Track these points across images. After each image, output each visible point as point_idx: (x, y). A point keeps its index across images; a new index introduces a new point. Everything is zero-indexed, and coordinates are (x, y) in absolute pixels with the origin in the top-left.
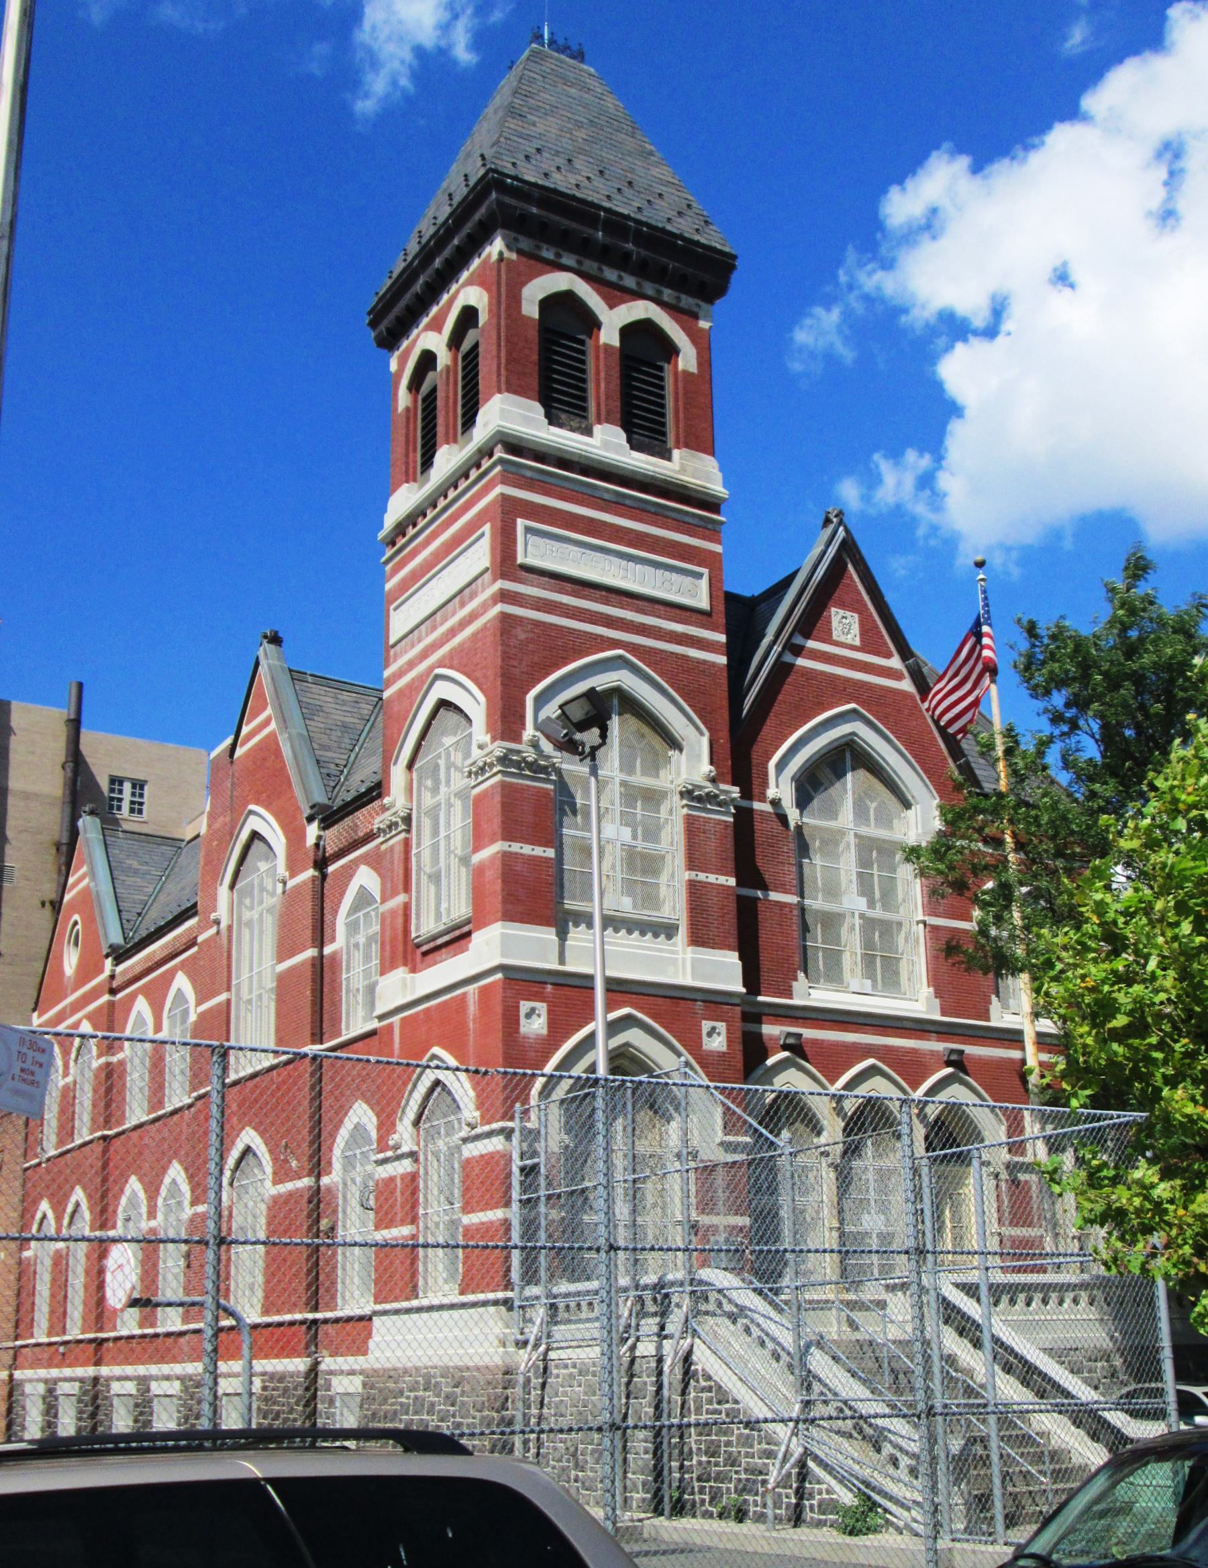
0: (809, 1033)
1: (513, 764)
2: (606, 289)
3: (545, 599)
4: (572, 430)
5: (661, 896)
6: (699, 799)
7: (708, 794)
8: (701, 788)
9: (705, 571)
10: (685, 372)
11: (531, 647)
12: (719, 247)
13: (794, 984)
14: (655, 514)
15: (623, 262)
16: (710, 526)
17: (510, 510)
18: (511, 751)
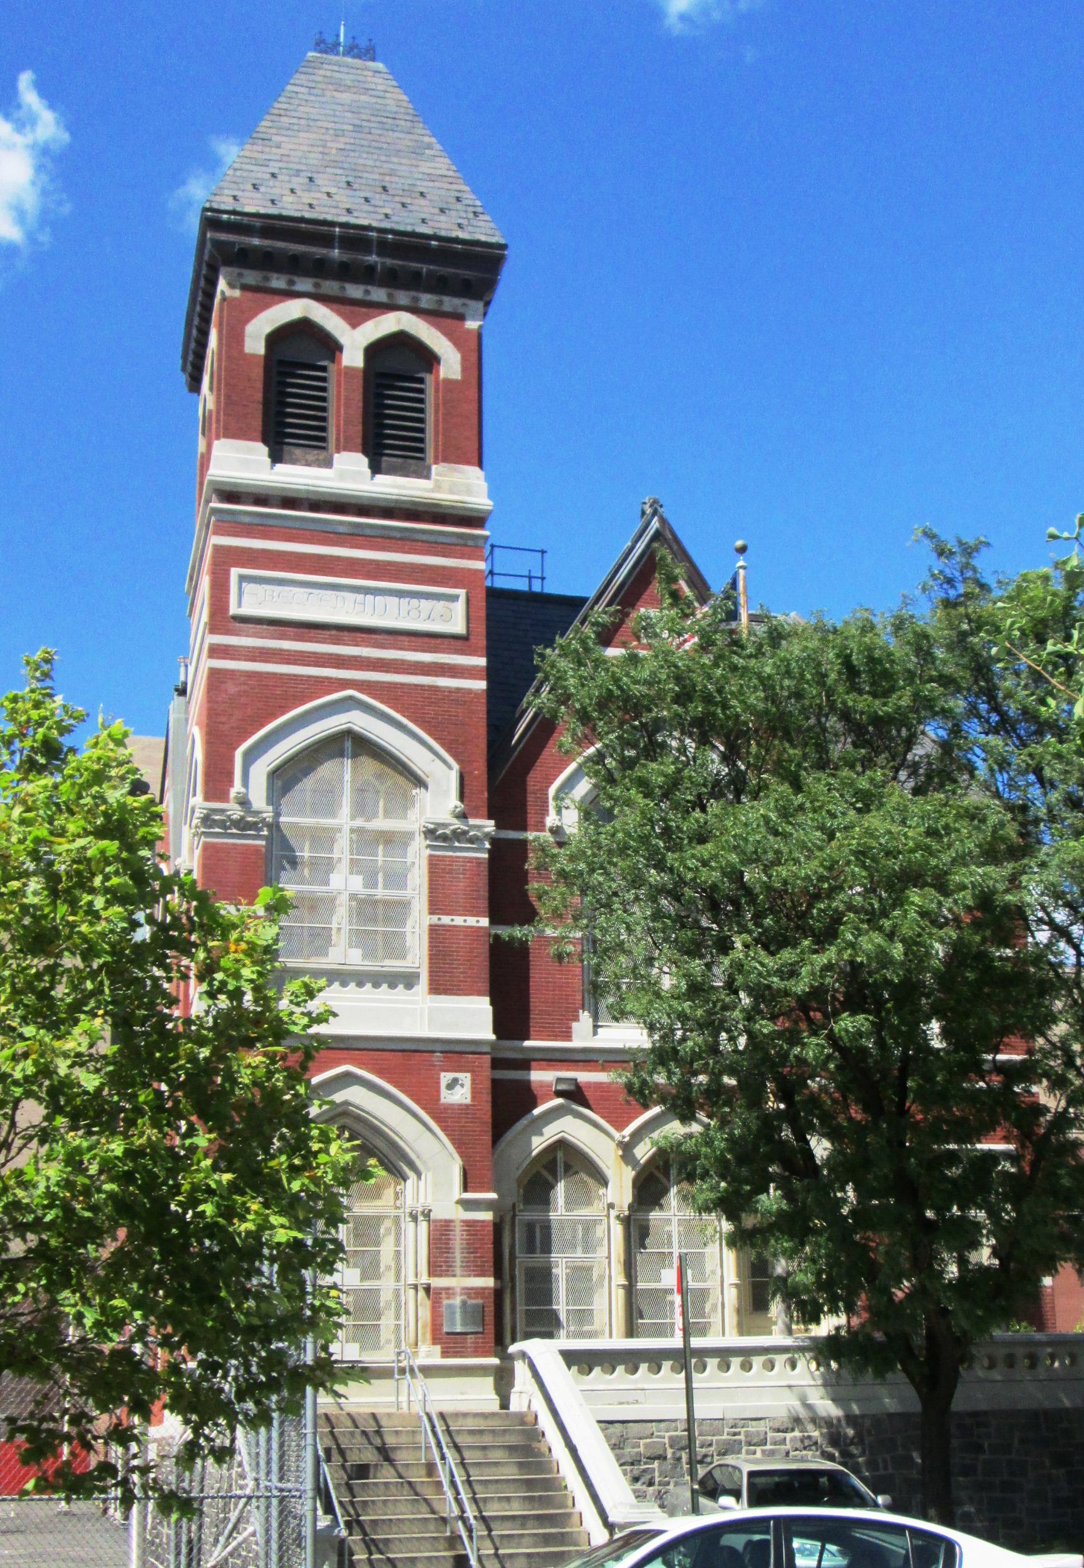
0: (584, 1077)
1: (215, 823)
2: (348, 308)
3: (263, 648)
4: (308, 464)
5: (408, 944)
6: (444, 838)
7: (454, 832)
8: (445, 825)
9: (462, 593)
10: (448, 381)
11: (243, 700)
12: (483, 238)
13: (574, 1025)
14: (401, 539)
15: (368, 275)
16: (470, 543)
17: (225, 559)
18: (215, 811)
